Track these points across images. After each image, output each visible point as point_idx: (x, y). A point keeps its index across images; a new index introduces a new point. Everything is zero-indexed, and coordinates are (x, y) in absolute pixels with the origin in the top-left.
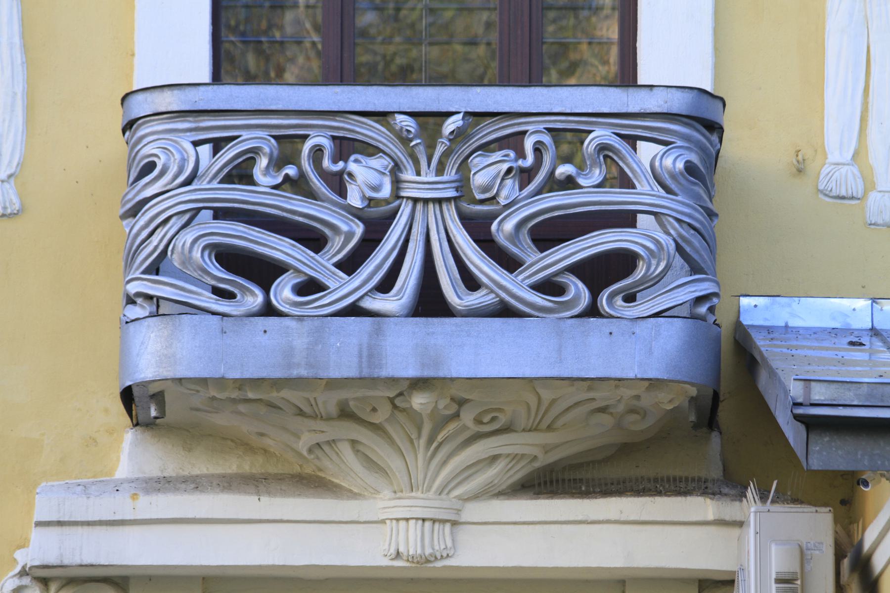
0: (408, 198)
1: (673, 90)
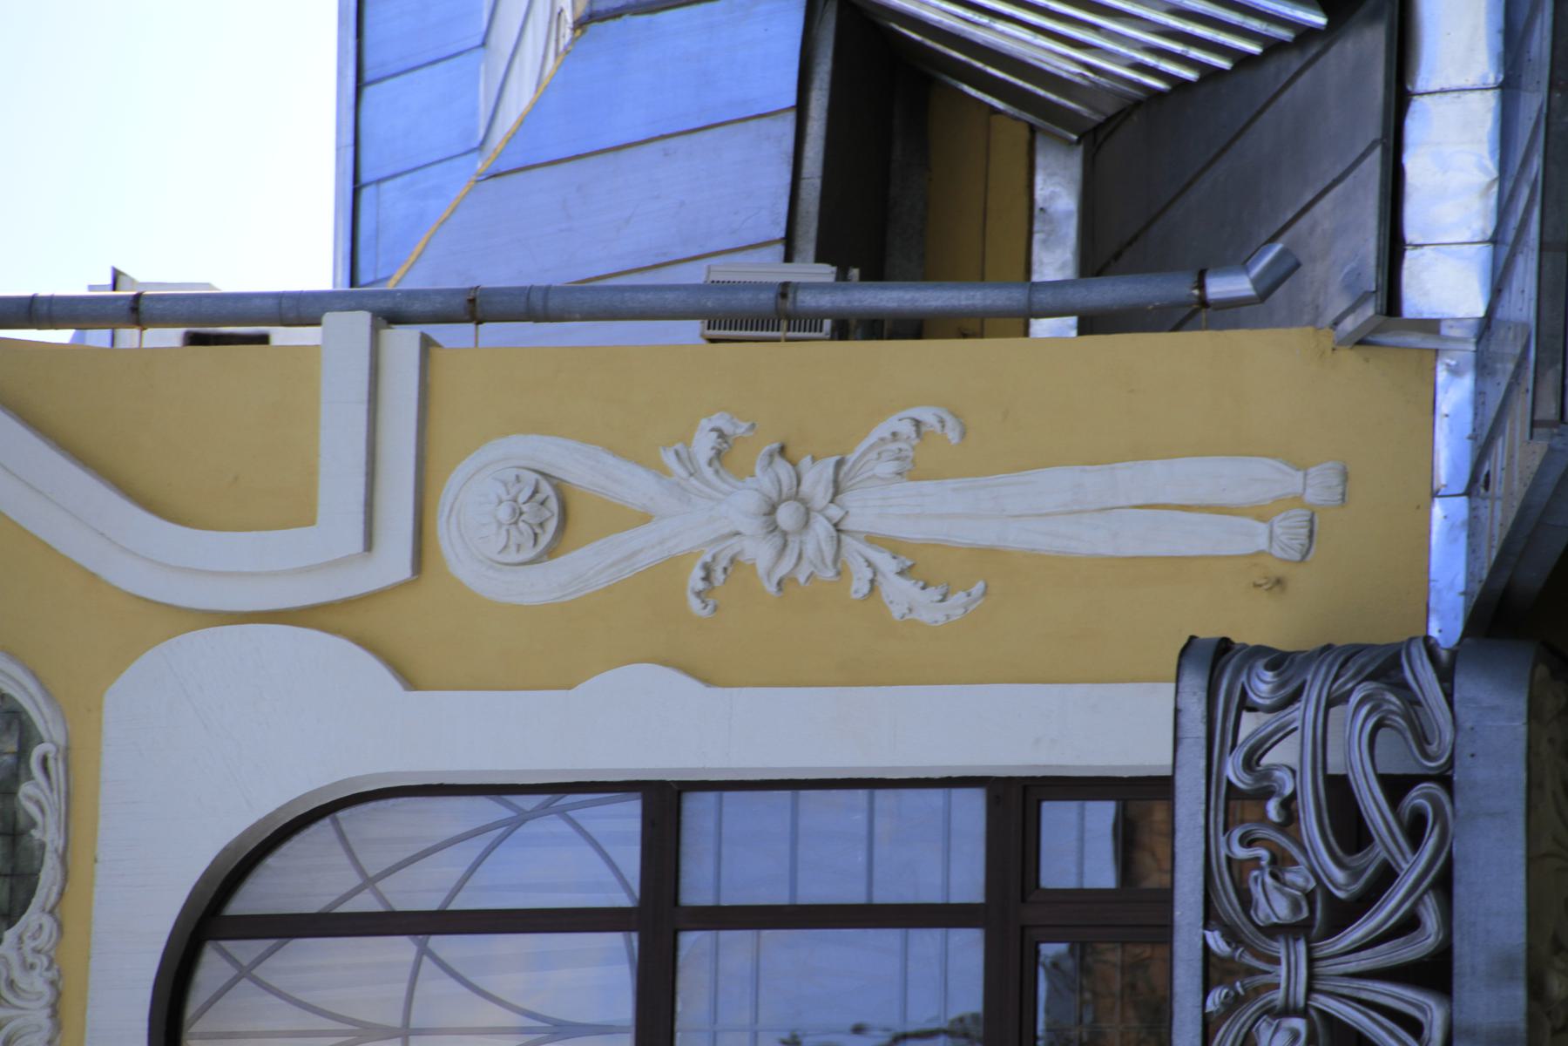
0: (1307, 997)
1: (1181, 685)
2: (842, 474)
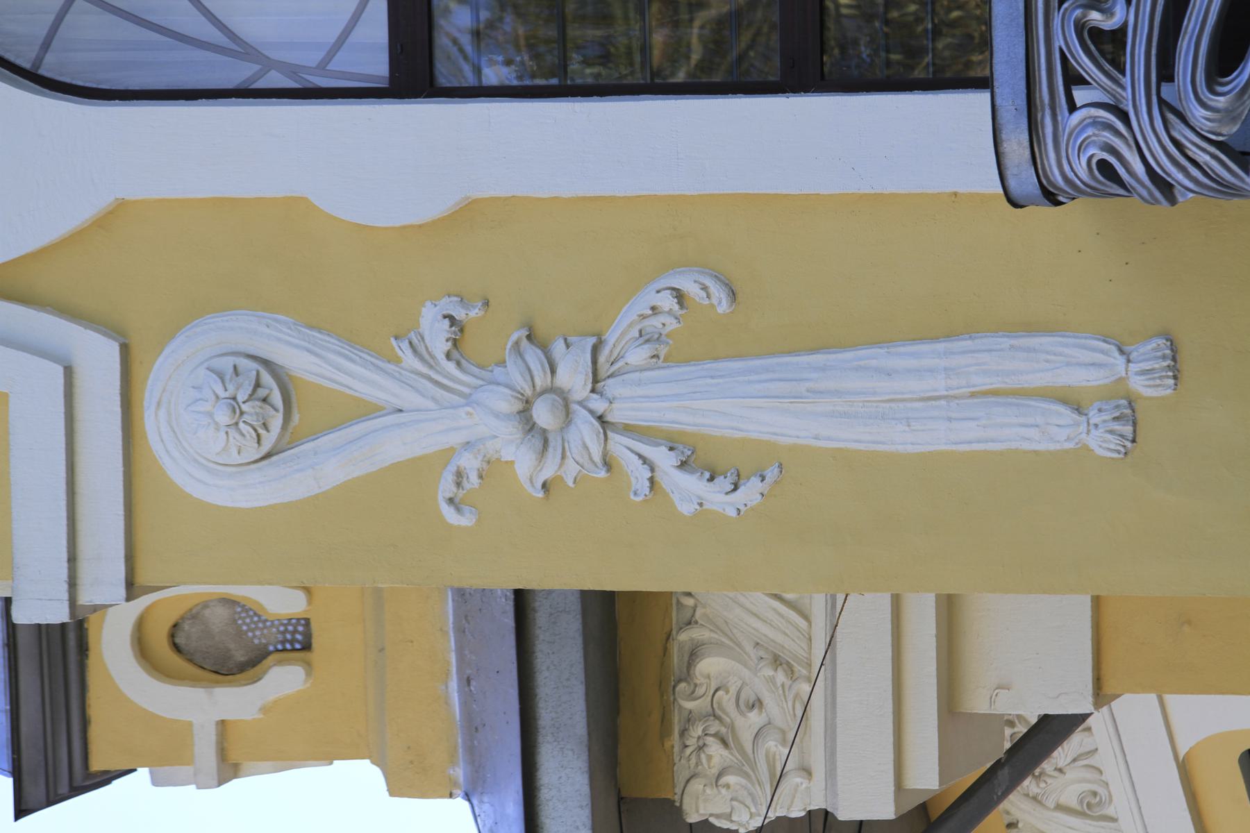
2: (602, 359)
